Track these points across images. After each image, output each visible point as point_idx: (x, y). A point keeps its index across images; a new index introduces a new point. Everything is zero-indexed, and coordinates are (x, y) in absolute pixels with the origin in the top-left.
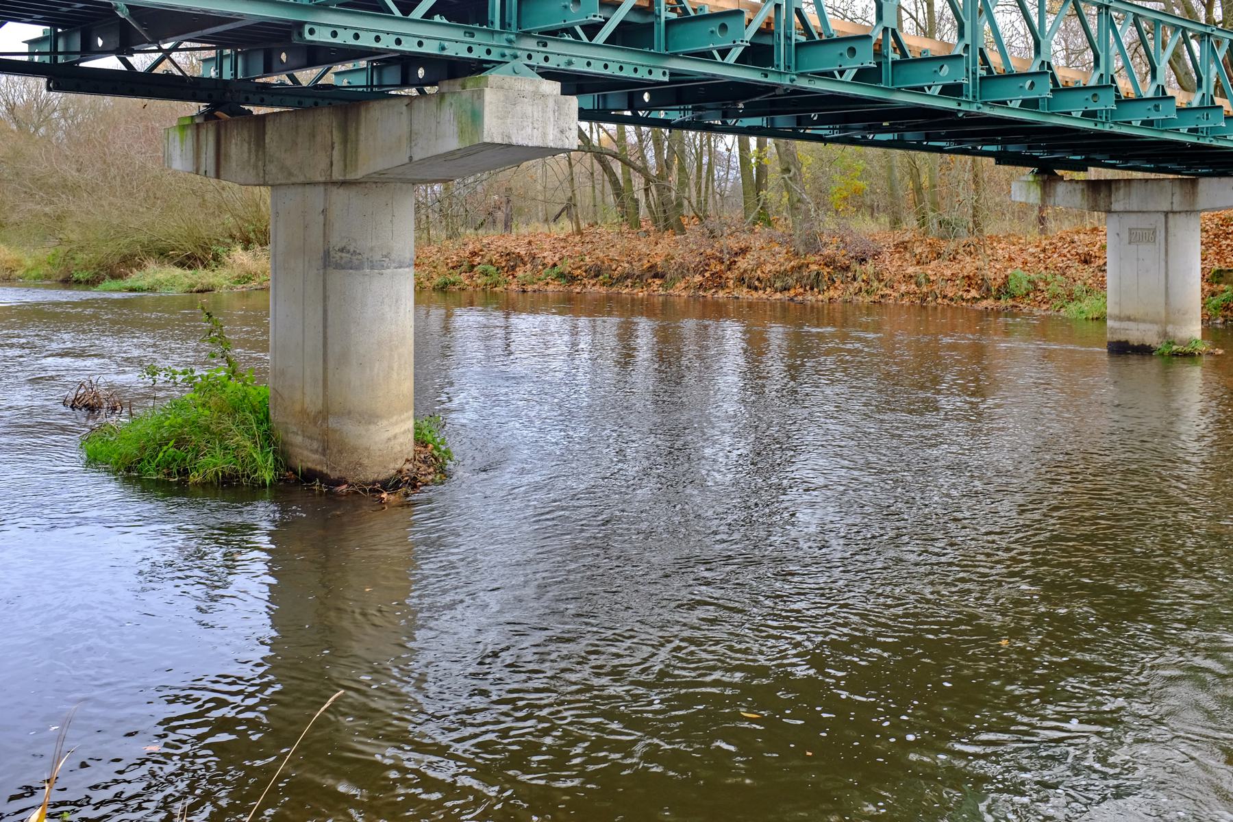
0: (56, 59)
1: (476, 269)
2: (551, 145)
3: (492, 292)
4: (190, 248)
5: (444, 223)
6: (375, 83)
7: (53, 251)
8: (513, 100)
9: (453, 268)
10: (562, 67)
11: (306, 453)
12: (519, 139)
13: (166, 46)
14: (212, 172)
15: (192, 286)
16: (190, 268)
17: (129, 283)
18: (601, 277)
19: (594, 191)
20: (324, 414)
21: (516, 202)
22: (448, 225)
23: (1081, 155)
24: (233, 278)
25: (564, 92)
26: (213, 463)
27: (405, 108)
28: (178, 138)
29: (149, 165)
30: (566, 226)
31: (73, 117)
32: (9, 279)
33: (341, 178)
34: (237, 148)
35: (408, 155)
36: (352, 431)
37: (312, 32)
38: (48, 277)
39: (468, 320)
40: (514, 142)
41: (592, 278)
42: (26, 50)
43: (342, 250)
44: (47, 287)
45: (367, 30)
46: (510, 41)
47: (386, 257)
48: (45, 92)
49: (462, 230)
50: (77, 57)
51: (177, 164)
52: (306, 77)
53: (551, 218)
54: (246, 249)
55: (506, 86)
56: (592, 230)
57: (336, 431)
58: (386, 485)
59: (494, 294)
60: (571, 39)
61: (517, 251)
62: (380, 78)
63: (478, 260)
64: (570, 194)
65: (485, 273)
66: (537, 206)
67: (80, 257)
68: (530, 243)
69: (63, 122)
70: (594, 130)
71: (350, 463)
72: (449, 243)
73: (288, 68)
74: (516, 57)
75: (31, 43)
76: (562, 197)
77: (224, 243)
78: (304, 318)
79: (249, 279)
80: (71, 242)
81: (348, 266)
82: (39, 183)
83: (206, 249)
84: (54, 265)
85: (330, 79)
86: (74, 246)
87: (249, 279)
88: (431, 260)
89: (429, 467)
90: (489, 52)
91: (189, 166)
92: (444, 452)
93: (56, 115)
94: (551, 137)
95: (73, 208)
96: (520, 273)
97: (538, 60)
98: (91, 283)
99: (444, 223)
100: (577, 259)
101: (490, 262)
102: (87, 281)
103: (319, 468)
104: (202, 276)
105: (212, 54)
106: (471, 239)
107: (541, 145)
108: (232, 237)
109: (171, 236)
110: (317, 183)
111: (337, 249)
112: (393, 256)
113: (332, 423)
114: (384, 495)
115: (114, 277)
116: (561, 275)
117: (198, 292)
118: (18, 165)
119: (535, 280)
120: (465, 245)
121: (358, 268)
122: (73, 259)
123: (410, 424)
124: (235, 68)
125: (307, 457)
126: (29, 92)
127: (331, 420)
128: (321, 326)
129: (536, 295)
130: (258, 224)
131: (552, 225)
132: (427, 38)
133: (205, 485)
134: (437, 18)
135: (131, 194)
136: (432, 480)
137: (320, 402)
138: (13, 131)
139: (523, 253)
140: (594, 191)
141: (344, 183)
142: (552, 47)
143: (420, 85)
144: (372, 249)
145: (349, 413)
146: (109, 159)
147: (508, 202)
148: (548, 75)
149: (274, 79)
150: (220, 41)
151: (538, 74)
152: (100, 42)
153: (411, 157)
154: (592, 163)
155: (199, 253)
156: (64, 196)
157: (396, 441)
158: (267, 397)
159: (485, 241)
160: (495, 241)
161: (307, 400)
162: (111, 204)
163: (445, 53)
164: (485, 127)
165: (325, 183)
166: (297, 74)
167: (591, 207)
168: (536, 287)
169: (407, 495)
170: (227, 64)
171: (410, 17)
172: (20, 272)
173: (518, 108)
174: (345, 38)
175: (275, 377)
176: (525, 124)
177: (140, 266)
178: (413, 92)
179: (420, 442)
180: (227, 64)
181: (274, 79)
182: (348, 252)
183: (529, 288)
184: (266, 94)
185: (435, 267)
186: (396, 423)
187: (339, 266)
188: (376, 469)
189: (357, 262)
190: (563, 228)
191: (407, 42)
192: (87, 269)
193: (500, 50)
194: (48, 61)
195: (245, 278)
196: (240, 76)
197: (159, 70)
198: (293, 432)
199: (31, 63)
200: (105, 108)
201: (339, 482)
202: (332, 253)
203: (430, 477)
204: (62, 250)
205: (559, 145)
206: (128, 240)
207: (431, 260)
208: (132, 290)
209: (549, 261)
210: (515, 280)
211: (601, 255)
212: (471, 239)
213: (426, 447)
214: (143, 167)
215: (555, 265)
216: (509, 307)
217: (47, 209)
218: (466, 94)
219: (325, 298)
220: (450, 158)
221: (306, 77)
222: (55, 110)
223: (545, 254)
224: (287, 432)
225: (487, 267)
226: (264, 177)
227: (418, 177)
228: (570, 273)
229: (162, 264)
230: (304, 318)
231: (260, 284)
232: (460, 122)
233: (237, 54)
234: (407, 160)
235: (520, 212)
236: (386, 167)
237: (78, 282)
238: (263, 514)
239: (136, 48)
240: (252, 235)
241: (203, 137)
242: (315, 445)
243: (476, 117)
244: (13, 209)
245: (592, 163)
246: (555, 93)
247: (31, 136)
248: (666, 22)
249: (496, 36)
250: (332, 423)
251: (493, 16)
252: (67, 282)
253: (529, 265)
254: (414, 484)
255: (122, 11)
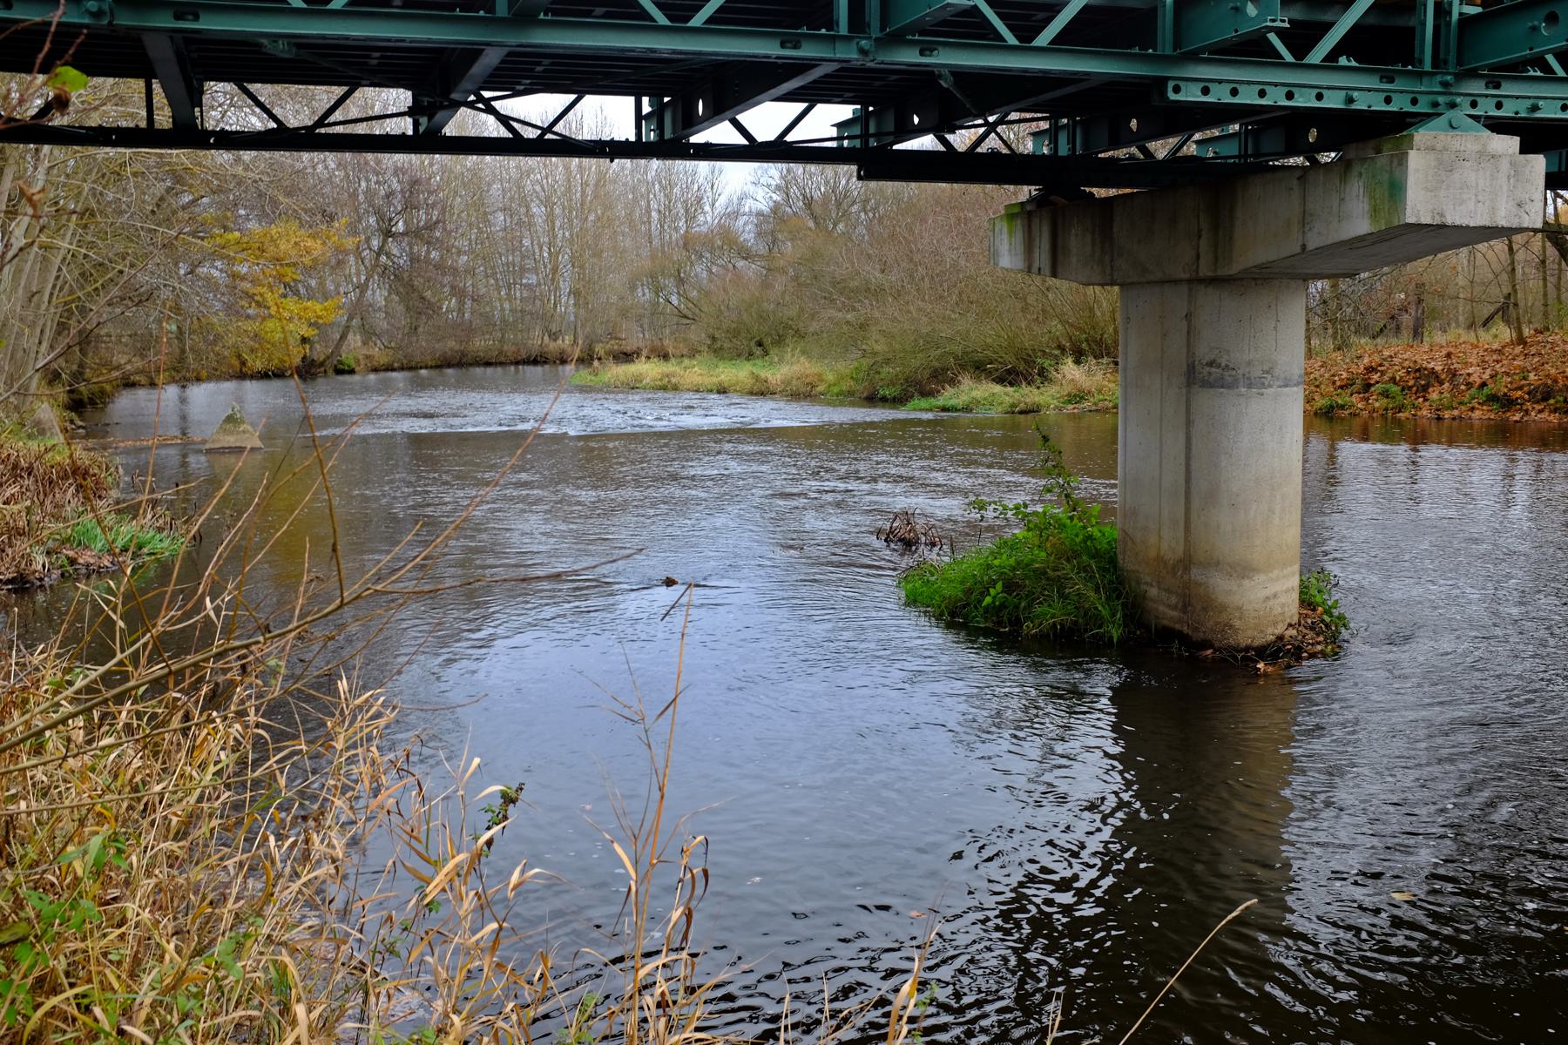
0: (867, 142)
1: (1373, 389)
2: (1503, 223)
3: (1394, 418)
4: (1010, 361)
5: (1330, 331)
6: (1250, 152)
7: (856, 364)
8: (1447, 165)
9: (1341, 387)
10: (1523, 115)
11: (1161, 608)
12: (1454, 217)
13: (991, 119)
14: (1047, 269)
15: (1013, 405)
16: (1011, 384)
17: (941, 401)
18: (1552, 401)
19: (1545, 286)
20: (1187, 562)
21: (1431, 302)
22: (1336, 333)
23: (320, 134)
24: (1062, 397)
25: (1524, 150)
26: (1049, 613)
27: (1295, 182)
28: (1005, 230)
29: (962, 262)
30: (1503, 333)
31: (874, 210)
32: (810, 396)
33: (1210, 274)
34: (1078, 242)
35: (1300, 243)
36: (1222, 587)
37: (1177, 90)
38: (850, 393)
39: (1351, 451)
40: (1449, 221)
41: (1538, 402)
42: (835, 135)
43: (1211, 364)
44: (852, 404)
45: (1276, 85)
46: (1445, 84)
47: (1267, 372)
48: (855, 179)
49: (1354, 339)
50: (891, 138)
51: (1006, 261)
52: (1161, 149)
53: (1479, 322)
54: (1077, 362)
55: (1439, 146)
56: (1540, 338)
57: (1200, 585)
58: (1263, 652)
59: (1398, 423)
60: (1539, 74)
61: (1431, 366)
62: (1256, 145)
63: (1376, 377)
64: (1510, 290)
65: (1385, 394)
66: (1456, 307)
67: (887, 371)
68: (1449, 355)
69: (862, 214)
70: (1550, 201)
71: (1217, 623)
72: (1338, 356)
73: (1140, 139)
74: (1453, 105)
75: (840, 126)
76: (1497, 294)
77: (1051, 355)
78: (1161, 446)
79: (1082, 398)
80: (875, 354)
81: (1220, 384)
82: (839, 286)
83: (1030, 362)
84: (856, 380)
85: (1191, 149)
86: (879, 359)
87: (1082, 398)
88: (1312, 376)
89: (1318, 635)
90: (1414, 102)
91: (1019, 263)
92: (1339, 618)
93: (855, 208)
94: (1503, 213)
95: (877, 314)
96: (1434, 396)
97: (1487, 108)
98: (898, 401)
99: (1330, 331)
100: (1517, 377)
101: (1393, 379)
102: (894, 398)
103: (1178, 627)
104: (1028, 394)
105: (1044, 125)
106: (1366, 350)
107: (1488, 224)
108: (1061, 348)
109: (988, 346)
110: (1181, 281)
111: (1204, 362)
112: (1277, 372)
113: (1196, 574)
114: (1261, 665)
115: (925, 394)
116: (1493, 398)
117: (1021, 412)
118: (816, 268)
119: (1454, 405)
120: (1358, 358)
121: (1232, 386)
122: (879, 373)
123: (1295, 582)
124: (1072, 141)
125: (1164, 608)
126: (827, 183)
127: (1194, 571)
128: (1183, 456)
129: (1455, 423)
130: (1092, 332)
131: (1481, 332)
132: (1329, 88)
133: (1041, 638)
134: (1343, 61)
135: (941, 297)
136: (1322, 652)
137: (1181, 548)
138: (810, 229)
139: (1438, 368)
140: (1545, 286)
141: (1215, 281)
142: (1508, 89)
143: (1310, 152)
144: (1249, 363)
145: (1218, 563)
146: (917, 258)
147: (1420, 301)
148: (1499, 126)
149: (1121, 153)
150: (1054, 110)
151: (1485, 126)
152: (916, 120)
153: (1304, 247)
154: (1544, 248)
155: (1022, 367)
156: (866, 301)
157: (1277, 601)
158: (1115, 540)
159: (1386, 353)
160: (1400, 352)
161: (1165, 546)
162: (920, 310)
163: (1354, 107)
164: (1409, 202)
165: (1190, 281)
166: (1152, 146)
167: (1539, 304)
168: (1456, 413)
169: (1289, 667)
170: (1063, 139)
171: (1307, 61)
172: (821, 388)
173: (1456, 176)
174: (1220, 95)
175: (1125, 516)
176: (1465, 196)
177: (953, 382)
178: (1299, 160)
179: (1307, 603)
180: (1063, 139)
181: (1121, 153)
182: (1219, 366)
183: (1447, 415)
184: (1112, 173)
185: (1317, 386)
186: (1277, 579)
187: (1208, 384)
188: (1249, 633)
189: (1230, 379)
190: (1496, 336)
191: (1301, 96)
192: (894, 385)
193: (1431, 97)
194: (858, 146)
195: (1078, 397)
196: (668, 135)
197: (983, 149)
198: (1146, 583)
199: (840, 148)
200: (910, 198)
201: (1207, 644)
202: (1198, 368)
203: (1319, 648)
204: (866, 362)
205: (1515, 224)
206: (939, 351)
207: (1312, 376)
208: (944, 409)
209: (1475, 379)
210: (1427, 404)
211: (1553, 371)
212: (1366, 350)
213: (1314, 610)
214: (955, 264)
215: (1484, 385)
216: (1418, 438)
217: (849, 316)
218: (1382, 160)
219: (1189, 423)
220: (1359, 245)
221: (1161, 149)
222: (854, 202)
223: (1470, 371)
224: (1138, 583)
225: (1388, 386)
226: (1112, 275)
227: (1312, 271)
228: (1505, 394)
229: (978, 379)
230: (1161, 446)
231: (1095, 404)
232: (1372, 198)
233: (1075, 123)
234: (1298, 250)
235: (1434, 314)
236: (1271, 259)
237: (884, 400)
238: (1102, 681)
239: (958, 123)
240: (1084, 345)
241: (1035, 227)
242: (1174, 600)
243: (1396, 190)
244: (812, 317)
245: (1544, 248)
246: (1511, 151)
247: (830, 233)
248: (1460, 21)
249: (1425, 80)
250: (1196, 574)
251: (1422, 51)
252: (872, 400)
253: (1446, 385)
254: (1297, 653)
255: (946, 80)
